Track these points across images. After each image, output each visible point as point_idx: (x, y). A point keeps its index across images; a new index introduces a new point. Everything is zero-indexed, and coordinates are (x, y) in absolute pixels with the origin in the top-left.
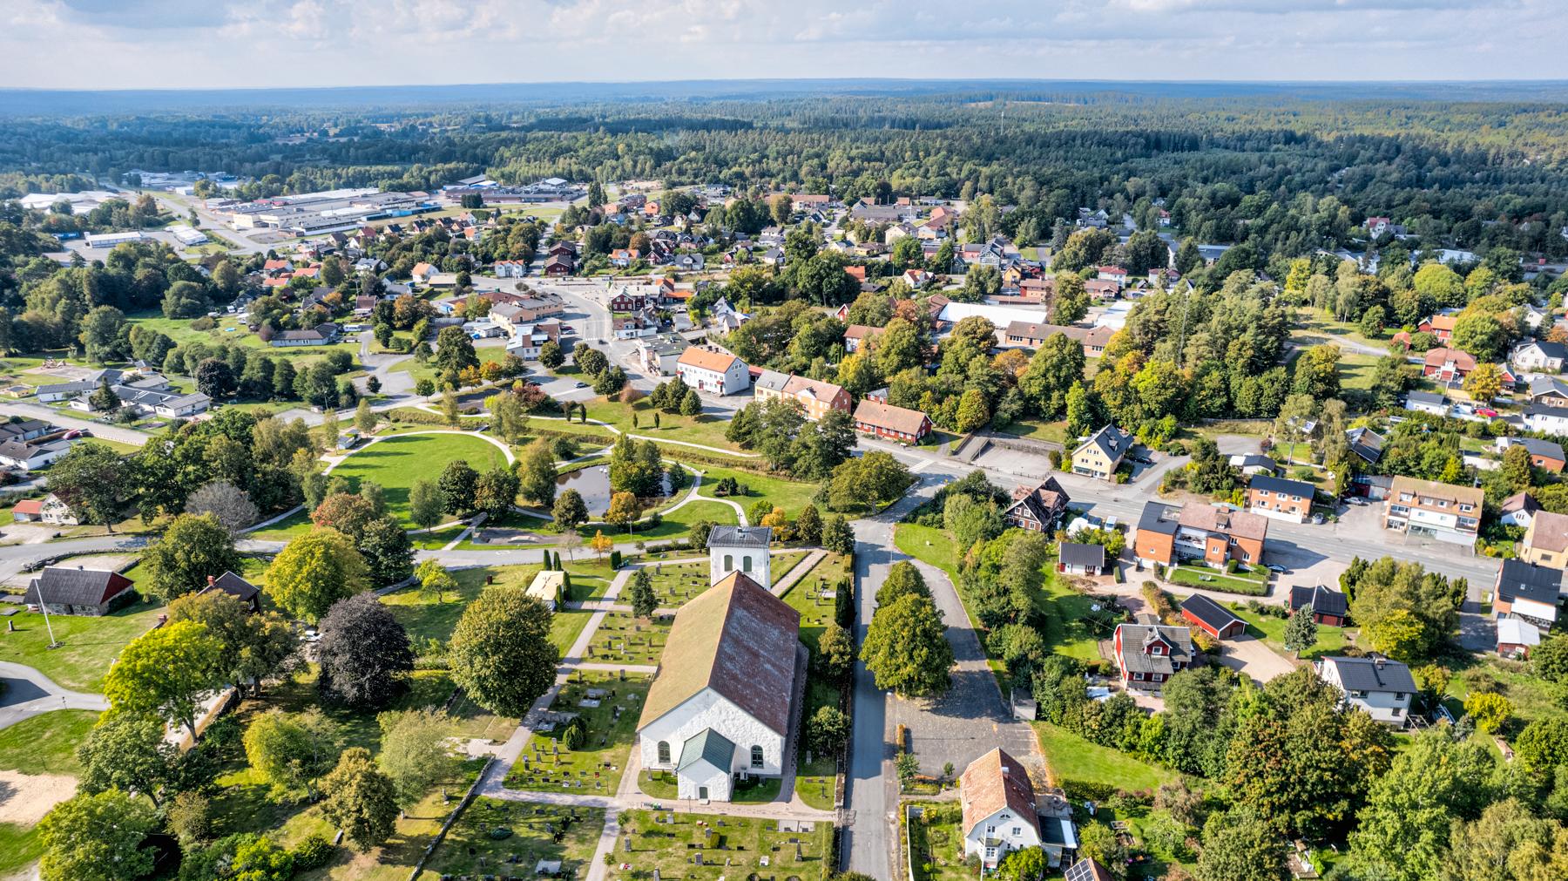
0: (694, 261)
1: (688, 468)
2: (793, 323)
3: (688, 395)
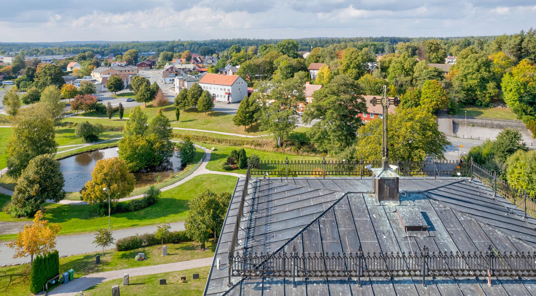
0: (213, 61)
1: (198, 147)
2: (275, 62)
3: (203, 94)
